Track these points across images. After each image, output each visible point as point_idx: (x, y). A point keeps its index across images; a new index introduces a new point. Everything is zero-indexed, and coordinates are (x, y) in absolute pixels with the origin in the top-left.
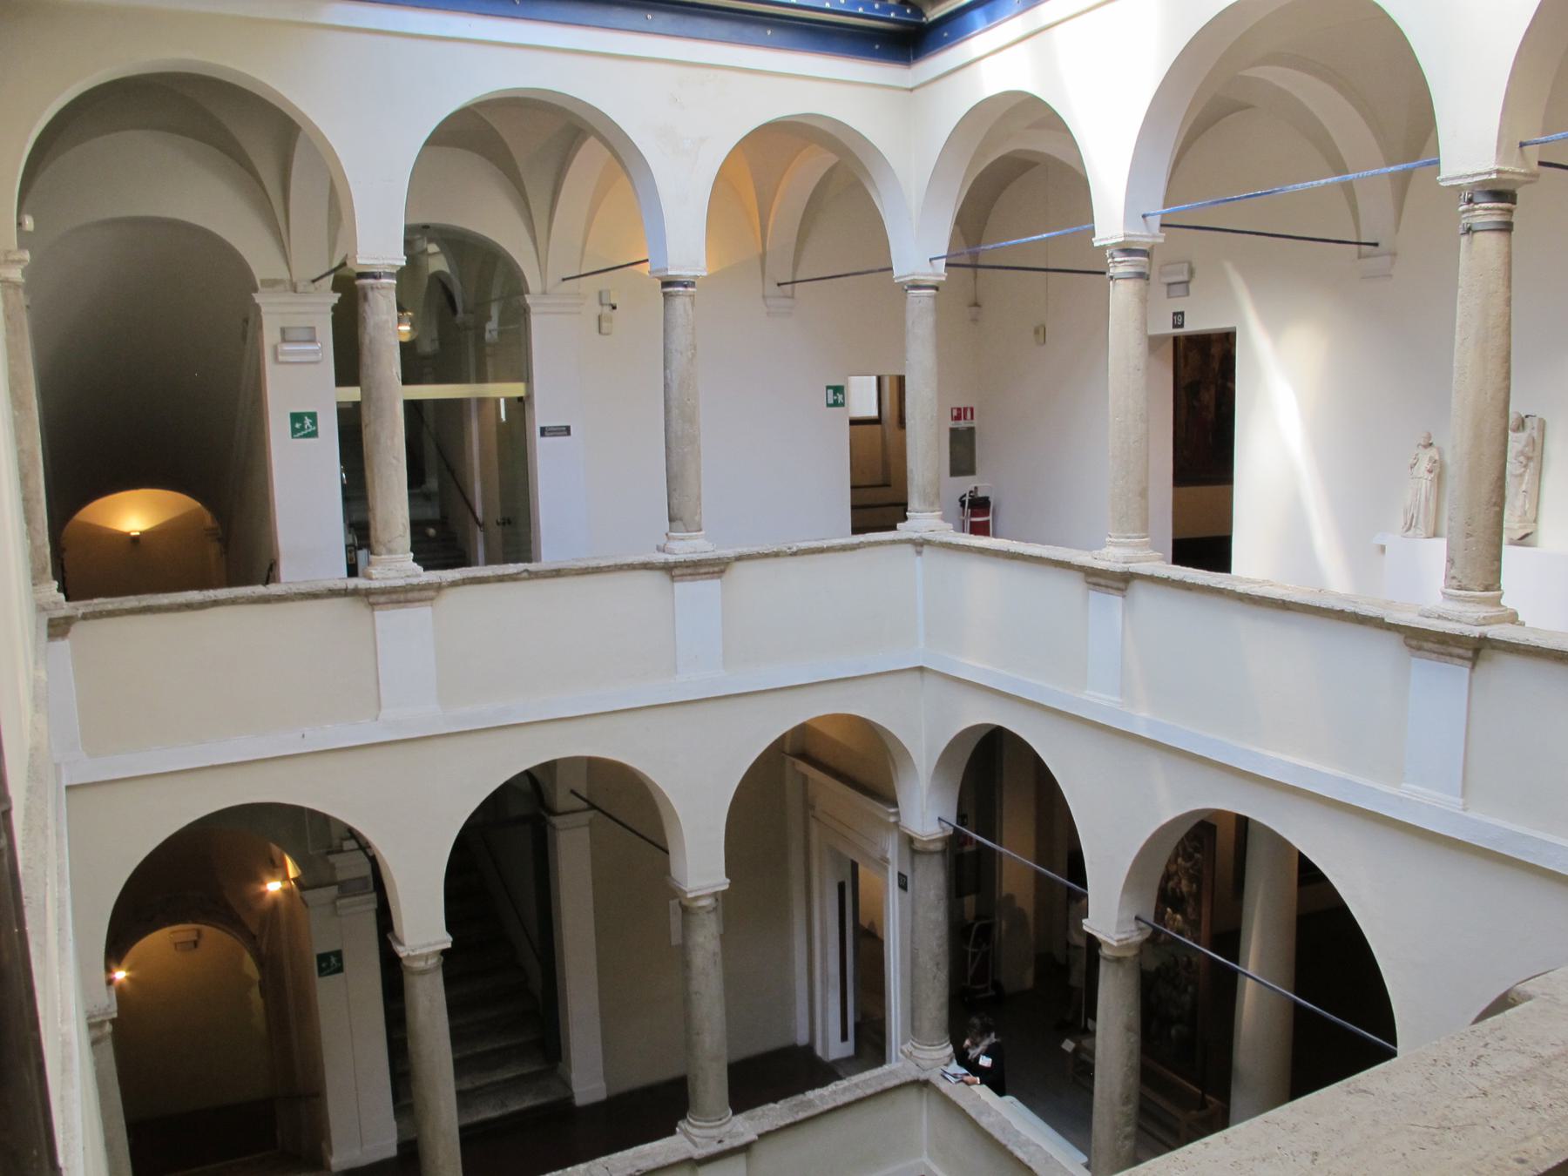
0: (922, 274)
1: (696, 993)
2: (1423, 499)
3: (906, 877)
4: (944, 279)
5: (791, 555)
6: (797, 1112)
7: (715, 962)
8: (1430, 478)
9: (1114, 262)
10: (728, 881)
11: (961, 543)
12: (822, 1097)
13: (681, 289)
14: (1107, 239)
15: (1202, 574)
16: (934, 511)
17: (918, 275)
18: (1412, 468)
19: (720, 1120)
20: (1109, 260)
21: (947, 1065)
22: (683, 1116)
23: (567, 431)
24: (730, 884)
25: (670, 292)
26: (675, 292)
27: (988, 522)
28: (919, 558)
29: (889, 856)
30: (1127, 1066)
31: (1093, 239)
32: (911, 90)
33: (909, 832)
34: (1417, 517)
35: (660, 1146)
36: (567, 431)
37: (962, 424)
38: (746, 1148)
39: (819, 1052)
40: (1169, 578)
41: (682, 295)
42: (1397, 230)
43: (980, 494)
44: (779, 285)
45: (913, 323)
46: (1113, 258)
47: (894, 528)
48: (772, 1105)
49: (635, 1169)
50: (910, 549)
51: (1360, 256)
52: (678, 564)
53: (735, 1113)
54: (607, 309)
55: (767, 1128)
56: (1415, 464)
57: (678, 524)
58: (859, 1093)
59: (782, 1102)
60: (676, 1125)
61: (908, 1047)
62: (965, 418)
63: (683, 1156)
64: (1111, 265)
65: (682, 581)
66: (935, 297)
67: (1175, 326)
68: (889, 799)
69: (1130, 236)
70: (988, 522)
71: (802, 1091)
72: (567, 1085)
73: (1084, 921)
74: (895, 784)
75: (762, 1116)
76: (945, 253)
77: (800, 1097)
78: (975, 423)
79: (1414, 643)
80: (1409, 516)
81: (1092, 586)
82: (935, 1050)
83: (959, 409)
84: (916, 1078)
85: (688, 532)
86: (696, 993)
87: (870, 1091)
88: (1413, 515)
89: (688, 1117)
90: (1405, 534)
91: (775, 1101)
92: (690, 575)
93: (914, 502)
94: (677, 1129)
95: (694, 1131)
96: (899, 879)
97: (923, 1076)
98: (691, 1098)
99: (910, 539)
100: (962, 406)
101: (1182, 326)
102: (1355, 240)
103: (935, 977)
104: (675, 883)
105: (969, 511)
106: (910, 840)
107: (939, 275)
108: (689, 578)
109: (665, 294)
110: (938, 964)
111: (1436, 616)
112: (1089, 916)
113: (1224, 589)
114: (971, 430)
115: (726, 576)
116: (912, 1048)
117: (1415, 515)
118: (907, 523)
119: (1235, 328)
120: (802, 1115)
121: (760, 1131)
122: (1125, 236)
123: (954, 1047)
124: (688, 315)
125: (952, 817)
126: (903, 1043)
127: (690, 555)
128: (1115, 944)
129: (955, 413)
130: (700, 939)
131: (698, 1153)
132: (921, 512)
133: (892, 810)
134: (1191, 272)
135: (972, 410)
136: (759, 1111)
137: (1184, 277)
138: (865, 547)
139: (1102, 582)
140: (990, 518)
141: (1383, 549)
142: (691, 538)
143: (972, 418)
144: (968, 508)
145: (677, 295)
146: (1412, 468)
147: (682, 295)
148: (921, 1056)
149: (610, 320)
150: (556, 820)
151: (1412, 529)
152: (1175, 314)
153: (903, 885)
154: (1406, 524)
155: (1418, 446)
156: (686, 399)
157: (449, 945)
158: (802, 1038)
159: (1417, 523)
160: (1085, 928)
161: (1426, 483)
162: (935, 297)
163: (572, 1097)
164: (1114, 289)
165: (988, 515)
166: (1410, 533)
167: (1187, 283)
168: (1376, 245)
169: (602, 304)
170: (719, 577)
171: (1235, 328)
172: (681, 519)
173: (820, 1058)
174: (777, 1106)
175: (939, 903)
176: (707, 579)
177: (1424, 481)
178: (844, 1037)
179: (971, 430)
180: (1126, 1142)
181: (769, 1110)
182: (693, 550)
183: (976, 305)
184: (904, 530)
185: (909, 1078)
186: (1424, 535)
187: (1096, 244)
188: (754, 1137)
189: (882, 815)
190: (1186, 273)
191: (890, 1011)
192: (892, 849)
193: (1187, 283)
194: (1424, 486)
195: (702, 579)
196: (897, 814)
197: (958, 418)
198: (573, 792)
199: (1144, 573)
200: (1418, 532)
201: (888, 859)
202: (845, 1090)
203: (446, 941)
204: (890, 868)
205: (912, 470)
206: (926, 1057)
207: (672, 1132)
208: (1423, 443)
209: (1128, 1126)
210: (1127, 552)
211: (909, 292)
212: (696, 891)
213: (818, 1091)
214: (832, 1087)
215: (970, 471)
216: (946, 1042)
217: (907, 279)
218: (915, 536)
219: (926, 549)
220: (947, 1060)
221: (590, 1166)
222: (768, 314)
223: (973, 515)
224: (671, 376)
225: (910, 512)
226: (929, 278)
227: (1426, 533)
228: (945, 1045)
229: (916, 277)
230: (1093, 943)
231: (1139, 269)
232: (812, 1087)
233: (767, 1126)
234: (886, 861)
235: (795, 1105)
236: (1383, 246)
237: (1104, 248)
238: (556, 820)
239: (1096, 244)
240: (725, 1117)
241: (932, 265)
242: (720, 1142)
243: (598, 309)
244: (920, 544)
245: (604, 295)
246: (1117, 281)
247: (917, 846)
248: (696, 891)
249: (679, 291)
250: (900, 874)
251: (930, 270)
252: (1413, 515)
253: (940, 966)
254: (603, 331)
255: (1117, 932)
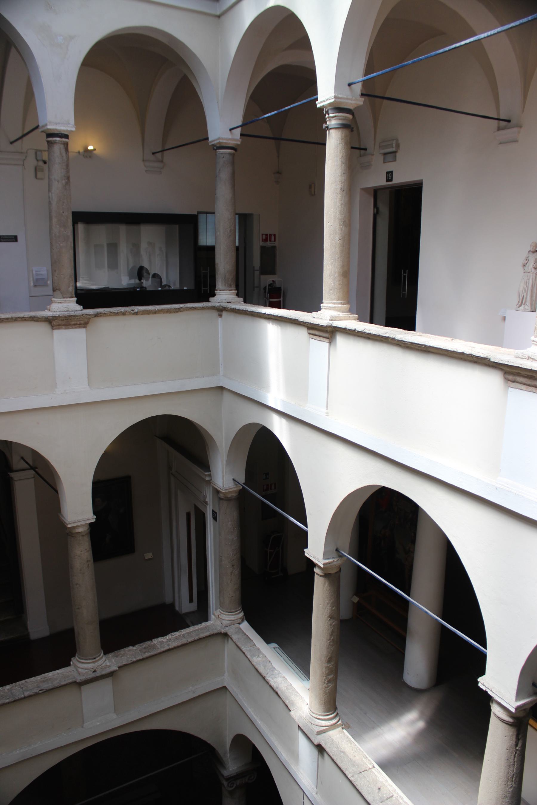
0: (225, 139)
1: (77, 584)
2: (530, 286)
3: (216, 513)
4: (239, 143)
5: (133, 314)
6: (145, 653)
7: (88, 566)
8: (535, 273)
9: (329, 117)
10: (95, 517)
11: (241, 309)
12: (161, 643)
13: (58, 139)
14: (324, 101)
15: (389, 329)
16: (231, 290)
17: (222, 139)
18: (524, 266)
19: (95, 658)
20: (327, 116)
21: (239, 624)
22: (74, 656)
23: (14, 239)
24: (96, 519)
25: (51, 141)
26: (53, 141)
27: (280, 301)
28: (220, 319)
29: (207, 500)
30: (330, 639)
31: (317, 102)
32: (219, 17)
33: (217, 488)
34: (526, 298)
35: (58, 674)
36: (14, 239)
37: (268, 244)
38: (111, 674)
39: (177, 608)
40: (355, 330)
41: (58, 143)
42: (523, 111)
43: (278, 285)
44: (153, 154)
45: (219, 170)
46: (329, 114)
47: (208, 301)
48: (131, 648)
49: (39, 689)
50: (215, 314)
51: (499, 129)
52: (55, 318)
53: (105, 653)
54: (41, 163)
55: (124, 663)
56: (526, 264)
57: (58, 292)
58: (184, 641)
59: (137, 646)
60: (70, 660)
61: (217, 613)
62: (270, 241)
63: (70, 681)
64: (327, 120)
65: (59, 329)
66: (233, 155)
67: (388, 180)
68: (205, 465)
69: (339, 98)
70: (280, 301)
71: (150, 638)
72: (25, 627)
73: (305, 550)
74: (209, 459)
75: (123, 655)
76: (240, 123)
77: (149, 643)
78: (276, 244)
79: (510, 377)
80: (521, 297)
81: (311, 336)
82: (233, 615)
83: (267, 235)
84: (220, 632)
85: (64, 298)
86: (77, 584)
87: (190, 640)
88: (523, 297)
89: (76, 656)
90: (518, 309)
91: (133, 645)
92: (64, 325)
93: (220, 284)
94: (71, 663)
95: (80, 665)
96: (213, 514)
97: (223, 631)
98: (77, 647)
99: (215, 307)
100: (269, 233)
101: (391, 180)
102: (496, 117)
103: (232, 573)
104: (61, 517)
105: (269, 294)
106: (217, 492)
107: (236, 140)
108: (63, 327)
109: (48, 142)
110: (233, 566)
111: (527, 357)
112: (308, 547)
113: (388, 337)
114: (274, 248)
115: (89, 326)
116: (220, 613)
117: (525, 296)
118: (215, 298)
119: (422, 180)
120: (147, 654)
121: (120, 665)
122: (335, 97)
123: (244, 613)
124: (63, 156)
125: (242, 479)
126: (216, 609)
127: (62, 313)
128: (322, 566)
129: (264, 237)
130: (78, 552)
131: (79, 679)
132: (223, 291)
133: (207, 473)
134: (398, 146)
135: (275, 235)
136: (122, 651)
137: (394, 149)
138: (183, 311)
139: (317, 333)
140: (282, 299)
141: (504, 318)
142: (65, 302)
143: (275, 241)
144: (268, 293)
145: (55, 142)
146: (524, 266)
147: (58, 143)
148: (224, 618)
149: (42, 170)
150: (12, 475)
151: (523, 305)
152: (388, 173)
153: (215, 518)
154: (519, 302)
155: (529, 252)
156: (61, 212)
157: (94, 520)
158: (168, 600)
159: (526, 302)
160: (306, 554)
161: (533, 276)
162: (233, 155)
163: (28, 635)
164: (329, 136)
165: (280, 298)
166: (521, 308)
167: (395, 152)
168: (509, 121)
169: (37, 160)
170: (85, 327)
171: (422, 180)
172: (59, 290)
173: (177, 611)
174: (134, 648)
175: (234, 530)
176: (76, 328)
177: (532, 274)
178: (191, 600)
179: (274, 248)
180: (330, 684)
181: (130, 650)
182: (66, 309)
183: (278, 173)
184: (214, 301)
185: (215, 632)
186: (529, 310)
187: (318, 106)
188: (116, 668)
189: (203, 477)
190: (394, 145)
191: (210, 589)
192: (209, 498)
193: (395, 152)
194: (531, 277)
195: (72, 328)
196: (210, 475)
197: (266, 240)
198: (22, 458)
199: (341, 327)
200: (526, 307)
201: (207, 502)
202: (177, 638)
203: (92, 518)
204: (208, 507)
205: (218, 264)
206: (226, 619)
207: (68, 665)
208: (532, 250)
209: (331, 674)
210: (335, 313)
211: (217, 150)
212: (73, 523)
213: (160, 639)
214: (168, 637)
215: (273, 272)
216: (240, 609)
217: (216, 142)
218: (217, 305)
219: (224, 314)
220: (239, 621)
221: (12, 688)
222: (146, 171)
223: (270, 298)
224: (52, 196)
225: (217, 290)
226: (229, 142)
227: (532, 308)
228: (240, 611)
229: (221, 141)
230: (311, 564)
231: (344, 122)
232: (157, 637)
233: (124, 661)
234: (206, 503)
235: (145, 648)
236: (513, 122)
237: (321, 109)
238: (12, 475)
239: (318, 106)
240: (98, 657)
241: (231, 133)
242: (94, 671)
243: (35, 163)
244: (220, 310)
245: (38, 153)
246: (331, 130)
247: (221, 496)
248: (73, 523)
249: (56, 140)
250: (213, 511)
251: (230, 137)
252: (523, 297)
253: (235, 566)
254: (38, 176)
255: (324, 559)
